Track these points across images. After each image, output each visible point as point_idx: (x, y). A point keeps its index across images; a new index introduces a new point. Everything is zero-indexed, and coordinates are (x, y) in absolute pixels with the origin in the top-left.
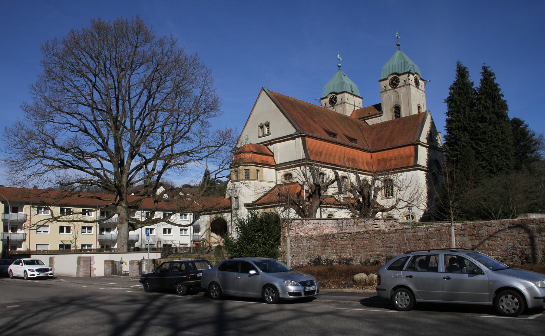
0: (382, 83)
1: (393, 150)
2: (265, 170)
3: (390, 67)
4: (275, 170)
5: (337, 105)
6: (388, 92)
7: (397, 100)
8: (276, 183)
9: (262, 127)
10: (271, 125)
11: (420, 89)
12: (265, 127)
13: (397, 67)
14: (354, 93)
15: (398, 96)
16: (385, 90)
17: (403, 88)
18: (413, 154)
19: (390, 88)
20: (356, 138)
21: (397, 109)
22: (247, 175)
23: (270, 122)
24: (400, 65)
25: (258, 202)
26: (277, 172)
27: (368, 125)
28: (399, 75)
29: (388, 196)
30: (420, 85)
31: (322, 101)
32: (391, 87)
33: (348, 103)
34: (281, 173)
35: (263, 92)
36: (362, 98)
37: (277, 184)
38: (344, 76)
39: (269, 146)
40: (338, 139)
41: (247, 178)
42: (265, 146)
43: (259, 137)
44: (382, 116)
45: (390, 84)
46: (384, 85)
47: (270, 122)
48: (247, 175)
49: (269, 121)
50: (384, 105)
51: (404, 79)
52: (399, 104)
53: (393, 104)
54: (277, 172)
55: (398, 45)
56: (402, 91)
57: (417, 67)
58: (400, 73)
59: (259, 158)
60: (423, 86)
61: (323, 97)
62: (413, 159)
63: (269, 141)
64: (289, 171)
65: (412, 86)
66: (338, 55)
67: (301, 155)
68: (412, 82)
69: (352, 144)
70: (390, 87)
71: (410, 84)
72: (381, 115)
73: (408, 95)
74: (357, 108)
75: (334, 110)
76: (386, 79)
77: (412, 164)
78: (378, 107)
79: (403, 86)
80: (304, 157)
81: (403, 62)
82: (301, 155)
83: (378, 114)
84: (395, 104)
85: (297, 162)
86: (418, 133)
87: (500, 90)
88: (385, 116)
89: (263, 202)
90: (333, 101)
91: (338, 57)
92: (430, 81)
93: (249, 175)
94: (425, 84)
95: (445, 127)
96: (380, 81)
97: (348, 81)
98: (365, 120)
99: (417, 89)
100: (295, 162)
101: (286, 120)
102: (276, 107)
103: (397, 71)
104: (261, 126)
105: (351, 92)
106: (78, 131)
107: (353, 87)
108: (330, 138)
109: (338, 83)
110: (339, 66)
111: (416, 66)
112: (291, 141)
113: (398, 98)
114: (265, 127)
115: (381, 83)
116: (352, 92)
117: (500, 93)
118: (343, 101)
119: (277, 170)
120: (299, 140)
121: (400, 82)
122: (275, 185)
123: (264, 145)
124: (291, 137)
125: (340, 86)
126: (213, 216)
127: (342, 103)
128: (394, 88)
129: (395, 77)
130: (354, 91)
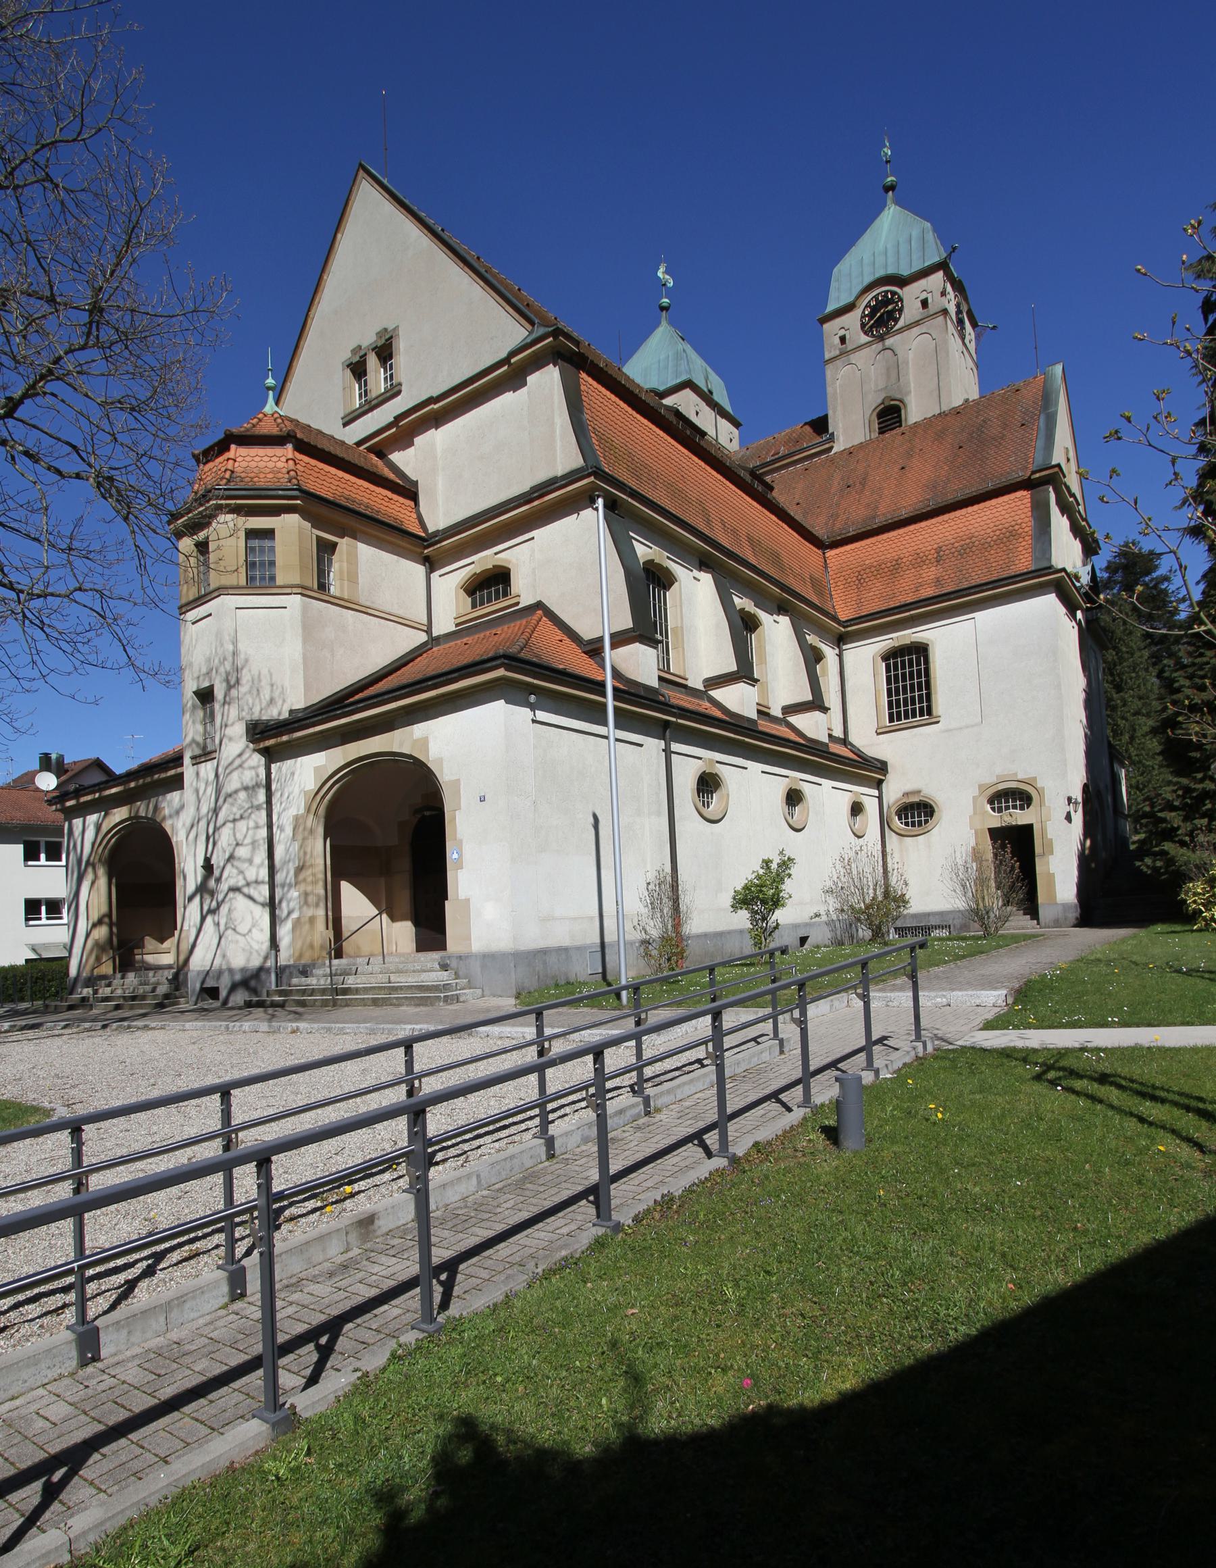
2: (366, 552)
3: (866, 261)
4: (420, 570)
6: (853, 358)
8: (429, 631)
9: (358, 370)
12: (372, 361)
13: (890, 253)
15: (895, 370)
17: (916, 331)
19: (865, 339)
24: (903, 249)
28: (902, 282)
29: (906, 717)
32: (866, 333)
36: (737, 424)
37: (435, 634)
39: (396, 457)
41: (262, 578)
46: (842, 332)
49: (391, 327)
52: (898, 396)
53: (874, 400)
54: (435, 576)
55: (891, 188)
58: (905, 272)
61: (831, 307)
64: (483, 560)
70: (862, 334)
73: (938, 354)
76: (849, 308)
77: (1024, 562)
79: (917, 323)
83: (813, 447)
84: (883, 395)
86: (1040, 443)
91: (660, 274)
92: (994, 328)
94: (978, 337)
103: (891, 271)
106: (236, 839)
109: (662, 357)
110: (662, 309)
112: (508, 397)
114: (372, 361)
119: (431, 564)
121: (906, 310)
122: (423, 637)
125: (671, 364)
126: (120, 814)
128: (881, 338)
129: (886, 292)
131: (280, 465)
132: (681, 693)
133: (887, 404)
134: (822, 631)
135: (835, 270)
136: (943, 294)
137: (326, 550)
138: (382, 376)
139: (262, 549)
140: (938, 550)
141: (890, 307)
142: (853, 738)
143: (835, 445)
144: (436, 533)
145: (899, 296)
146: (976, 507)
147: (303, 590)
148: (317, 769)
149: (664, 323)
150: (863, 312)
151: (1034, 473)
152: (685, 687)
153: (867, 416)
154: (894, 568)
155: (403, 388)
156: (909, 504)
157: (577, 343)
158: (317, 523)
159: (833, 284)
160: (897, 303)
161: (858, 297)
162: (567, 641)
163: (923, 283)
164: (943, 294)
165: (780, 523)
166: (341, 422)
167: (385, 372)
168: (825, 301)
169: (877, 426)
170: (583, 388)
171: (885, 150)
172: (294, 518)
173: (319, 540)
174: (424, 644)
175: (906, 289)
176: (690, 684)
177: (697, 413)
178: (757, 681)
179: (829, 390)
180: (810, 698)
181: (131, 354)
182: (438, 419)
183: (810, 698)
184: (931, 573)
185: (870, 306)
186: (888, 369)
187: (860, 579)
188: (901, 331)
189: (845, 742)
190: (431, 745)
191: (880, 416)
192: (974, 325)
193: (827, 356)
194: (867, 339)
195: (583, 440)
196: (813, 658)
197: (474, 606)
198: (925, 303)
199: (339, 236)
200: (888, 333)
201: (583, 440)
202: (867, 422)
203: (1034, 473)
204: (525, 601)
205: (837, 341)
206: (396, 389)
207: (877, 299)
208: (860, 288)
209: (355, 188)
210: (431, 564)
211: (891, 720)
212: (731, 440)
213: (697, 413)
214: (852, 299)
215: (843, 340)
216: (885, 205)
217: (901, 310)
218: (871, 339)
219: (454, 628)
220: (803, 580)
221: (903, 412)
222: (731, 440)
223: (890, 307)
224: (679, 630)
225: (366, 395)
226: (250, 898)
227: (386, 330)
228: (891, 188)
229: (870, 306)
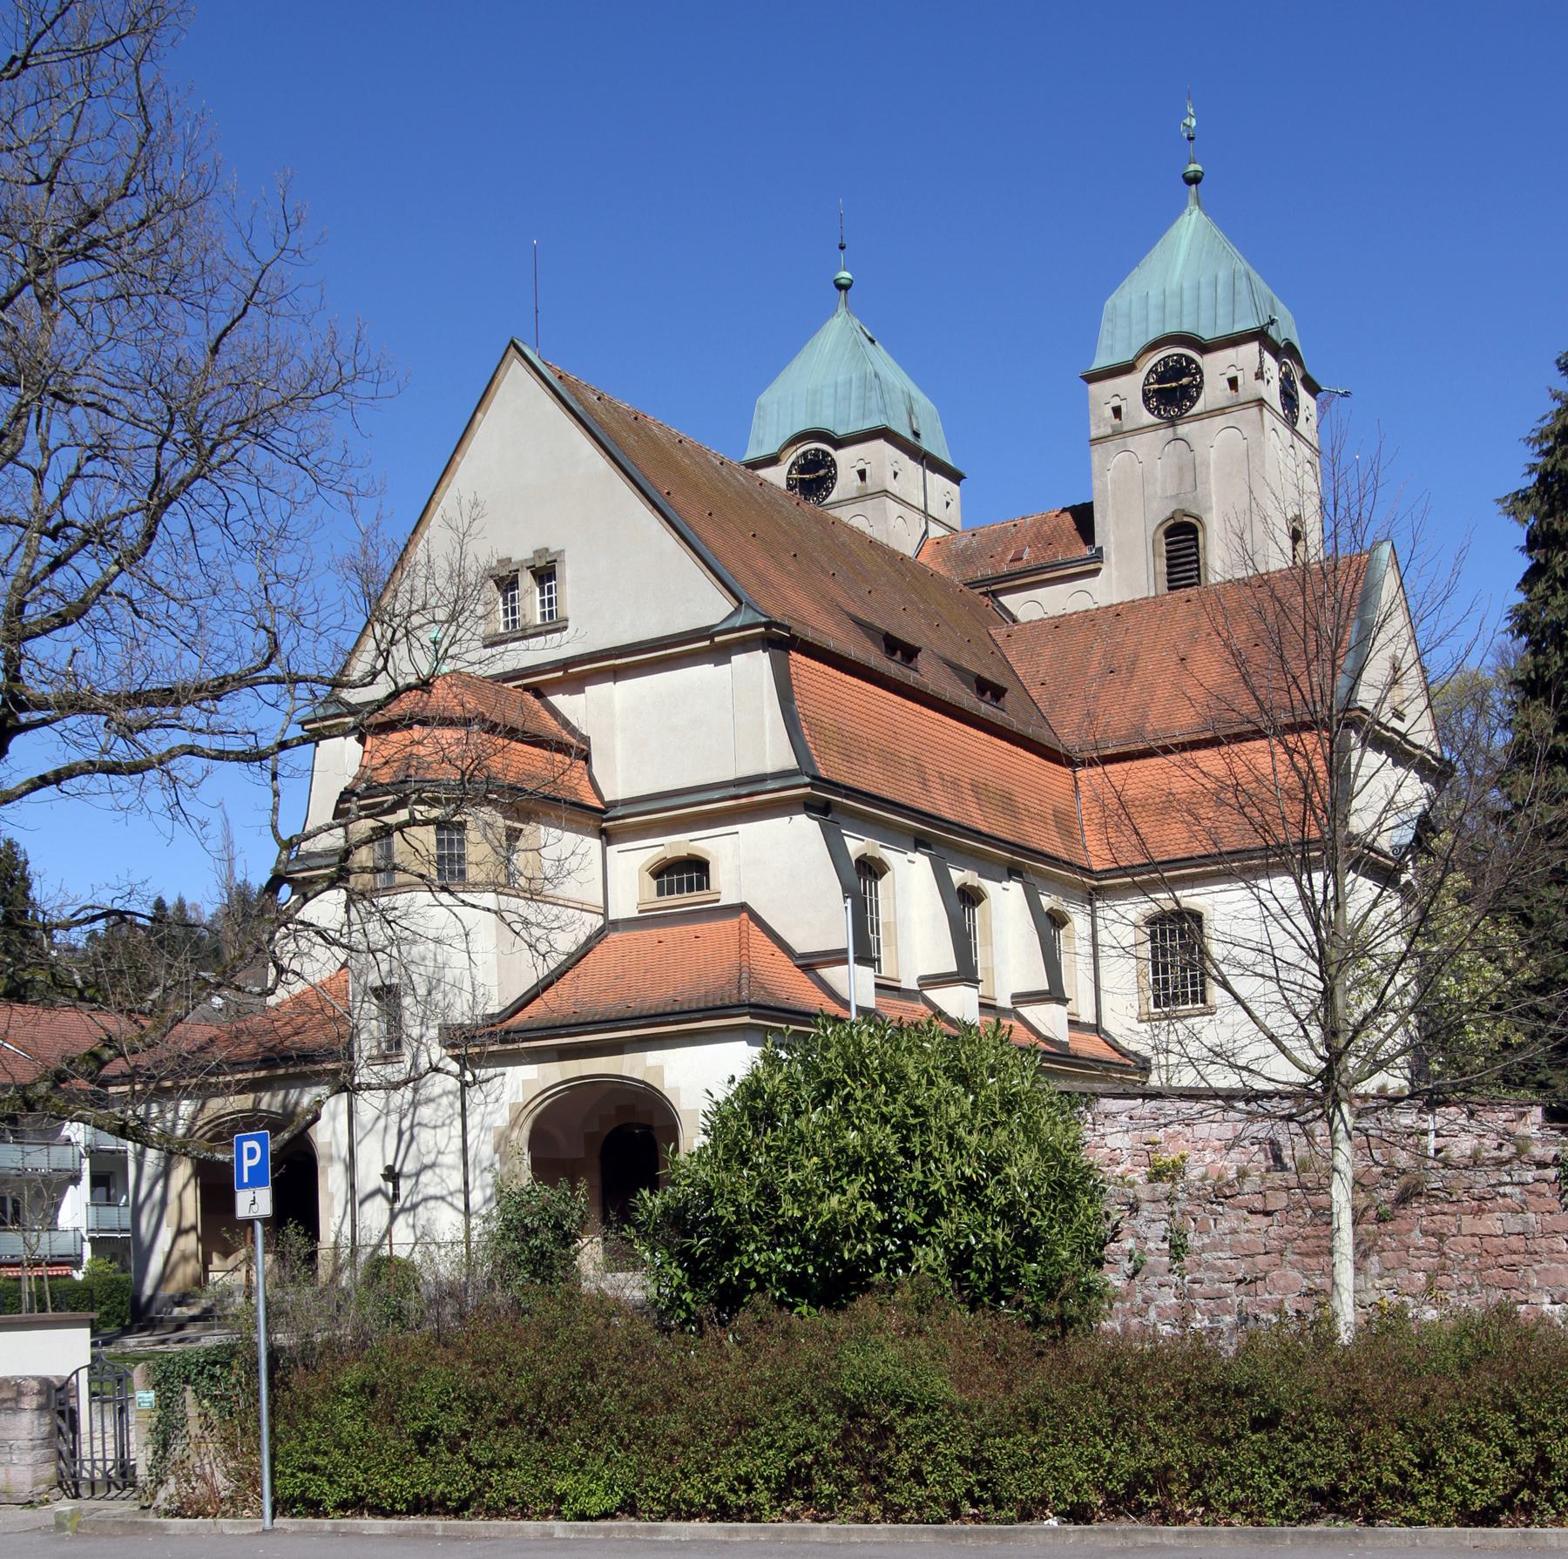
0: (1102, 391)
3: (1153, 301)
4: (595, 844)
6: (1133, 442)
7: (1188, 487)
8: (605, 914)
9: (507, 584)
10: (569, 573)
12: (526, 580)
13: (1187, 296)
14: (926, 444)
15: (1191, 471)
16: (1117, 433)
17: (1219, 421)
22: (451, 861)
23: (561, 552)
24: (1206, 293)
25: (520, 1016)
26: (612, 850)
27: (1015, 621)
30: (1302, 415)
35: (516, 371)
36: (955, 477)
37: (612, 916)
38: (872, 341)
39: (559, 700)
42: (529, 697)
43: (492, 642)
44: (1095, 572)
45: (1146, 400)
46: (1116, 402)
47: (561, 552)
48: (451, 861)
50: (1110, 519)
51: (1232, 373)
52: (1195, 511)
53: (1161, 511)
55: (1193, 180)
58: (1207, 334)
59: (524, 762)
60: (1314, 421)
61: (1101, 361)
63: (565, 664)
67: (776, 754)
68: (1272, 393)
69: (985, 709)
70: (1146, 412)
71: (1261, 402)
72: (1092, 567)
73: (1251, 457)
74: (936, 531)
76: (1127, 369)
78: (1083, 517)
79: (1221, 411)
80: (791, 762)
82: (776, 754)
84: (1173, 507)
85: (744, 791)
88: (1115, 574)
89: (608, 1003)
92: (1346, 395)
93: (461, 857)
94: (1321, 408)
95: (181, 906)
96: (1092, 378)
98: (995, 595)
100: (733, 791)
101: (669, 541)
102: (602, 463)
103: (1187, 327)
104: (540, 563)
105: (911, 438)
107: (916, 408)
108: (892, 668)
109: (840, 379)
110: (841, 287)
111: (923, 403)
112: (705, 671)
113: (1189, 478)
114: (526, 580)
115: (1094, 388)
116: (916, 435)
118: (871, 484)
123: (526, 688)
124: (707, 643)
128: (1172, 422)
129: (1182, 356)
130: (922, 433)
132: (893, 997)
133: (1178, 519)
134: (1065, 889)
135: (1108, 303)
136: (1259, 375)
137: (513, 835)
138: (538, 598)
139: (451, 842)
141: (1185, 381)
142: (1107, 1024)
143: (1103, 566)
144: (613, 804)
145: (1198, 367)
148: (525, 1082)
149: (842, 310)
150: (1147, 378)
152: (898, 989)
153: (1150, 532)
155: (570, 624)
157: (788, 629)
159: (1105, 326)
160: (1193, 375)
161: (1139, 357)
162: (778, 952)
163: (1229, 354)
164: (1259, 375)
165: (1014, 748)
167: (542, 593)
168: (1091, 357)
170: (793, 670)
171: (1187, 121)
173: (509, 828)
176: (903, 985)
177: (896, 474)
178: (978, 982)
180: (1046, 987)
181: (16, 357)
182: (616, 674)
183: (1046, 987)
185: (1156, 372)
186: (1181, 469)
188: (1199, 417)
189: (1097, 1028)
190: (666, 1074)
191: (1168, 534)
192: (1313, 389)
193: (1094, 433)
194: (1152, 419)
195: (795, 738)
196: (1051, 924)
197: (660, 893)
198: (1233, 383)
199: (479, 415)
200: (1180, 417)
201: (795, 738)
202: (1150, 540)
204: (726, 900)
205: (1110, 413)
206: (561, 625)
207: (1166, 364)
209: (503, 368)
210: (608, 837)
211: (1157, 1005)
213: (896, 474)
214: (1130, 357)
215: (1117, 412)
216: (1185, 206)
217: (1199, 387)
218: (1158, 421)
219: (636, 914)
220: (1044, 820)
221: (1200, 535)
224: (891, 925)
225: (514, 613)
226: (451, 1205)
227: (547, 550)
228: (1193, 180)
229: (1156, 372)
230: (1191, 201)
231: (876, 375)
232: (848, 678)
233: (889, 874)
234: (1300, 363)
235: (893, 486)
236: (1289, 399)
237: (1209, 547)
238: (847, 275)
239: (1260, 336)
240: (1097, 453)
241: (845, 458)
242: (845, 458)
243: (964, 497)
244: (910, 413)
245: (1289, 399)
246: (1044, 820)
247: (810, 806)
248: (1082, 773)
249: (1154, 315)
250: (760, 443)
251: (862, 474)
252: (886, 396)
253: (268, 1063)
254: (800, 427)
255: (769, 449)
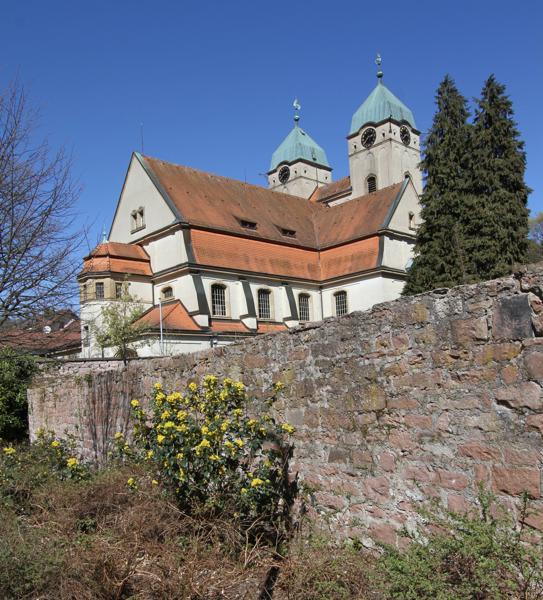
0: (351, 141)
1: (349, 245)
3: (365, 113)
4: (150, 285)
5: (290, 181)
6: (360, 155)
9: (135, 217)
10: (146, 213)
11: (410, 148)
12: (138, 215)
14: (317, 162)
15: (373, 162)
16: (355, 153)
17: (380, 146)
18: (377, 250)
20: (291, 228)
21: (372, 181)
28: (376, 126)
31: (270, 177)
33: (305, 178)
34: (159, 288)
36: (329, 170)
38: (304, 134)
40: (258, 232)
42: (139, 247)
44: (350, 194)
46: (355, 144)
51: (383, 132)
53: (366, 174)
54: (155, 286)
55: (380, 76)
56: (378, 151)
57: (408, 110)
61: (352, 133)
62: (376, 257)
64: (166, 284)
65: (395, 141)
66: (295, 102)
68: (398, 137)
69: (286, 238)
71: (391, 140)
74: (320, 185)
75: (285, 191)
76: (357, 134)
77: (374, 265)
81: (382, 104)
87: (515, 133)
90: (284, 176)
91: (295, 105)
93: (103, 292)
97: (308, 142)
98: (327, 203)
99: (404, 147)
101: (163, 202)
103: (372, 120)
105: (312, 161)
107: (315, 152)
108: (244, 230)
110: (296, 120)
112: (171, 237)
114: (138, 215)
116: (315, 159)
117: (519, 139)
119: (154, 283)
120: (180, 234)
122: (152, 305)
123: (137, 244)
127: (296, 178)
128: (368, 148)
129: (370, 129)
130: (317, 159)
131: (105, 263)
139: (100, 288)
140: (352, 256)
141: (371, 136)
146: (364, 241)
147: (112, 299)
151: (379, 231)
154: (339, 261)
156: (347, 236)
157: (188, 223)
158: (115, 279)
159: (353, 122)
161: (360, 130)
166: (130, 233)
168: (349, 131)
169: (368, 185)
171: (378, 59)
172: (109, 279)
174: (152, 307)
175: (378, 128)
179: (350, 168)
182: (155, 239)
184: (349, 264)
187: (330, 264)
188: (375, 146)
193: (350, 154)
198: (384, 134)
200: (370, 146)
203: (379, 231)
205: (353, 147)
208: (361, 125)
210: (154, 283)
212: (326, 178)
214: (357, 131)
215: (355, 147)
217: (375, 137)
222: (326, 178)
223: (371, 136)
230: (379, 82)
231: (300, 144)
232: (217, 234)
233: (227, 288)
234: (410, 126)
235: (303, 174)
236: (406, 139)
237: (379, 183)
238: (297, 117)
239: (390, 120)
240: (351, 159)
241: (292, 168)
242: (292, 168)
243: (332, 174)
244: (313, 153)
245: (406, 139)
246: (303, 268)
247: (190, 272)
248: (321, 253)
249: (365, 117)
250: (273, 166)
251: (296, 172)
252: (303, 150)
253: (69, 347)
254: (282, 160)
255: (275, 168)
